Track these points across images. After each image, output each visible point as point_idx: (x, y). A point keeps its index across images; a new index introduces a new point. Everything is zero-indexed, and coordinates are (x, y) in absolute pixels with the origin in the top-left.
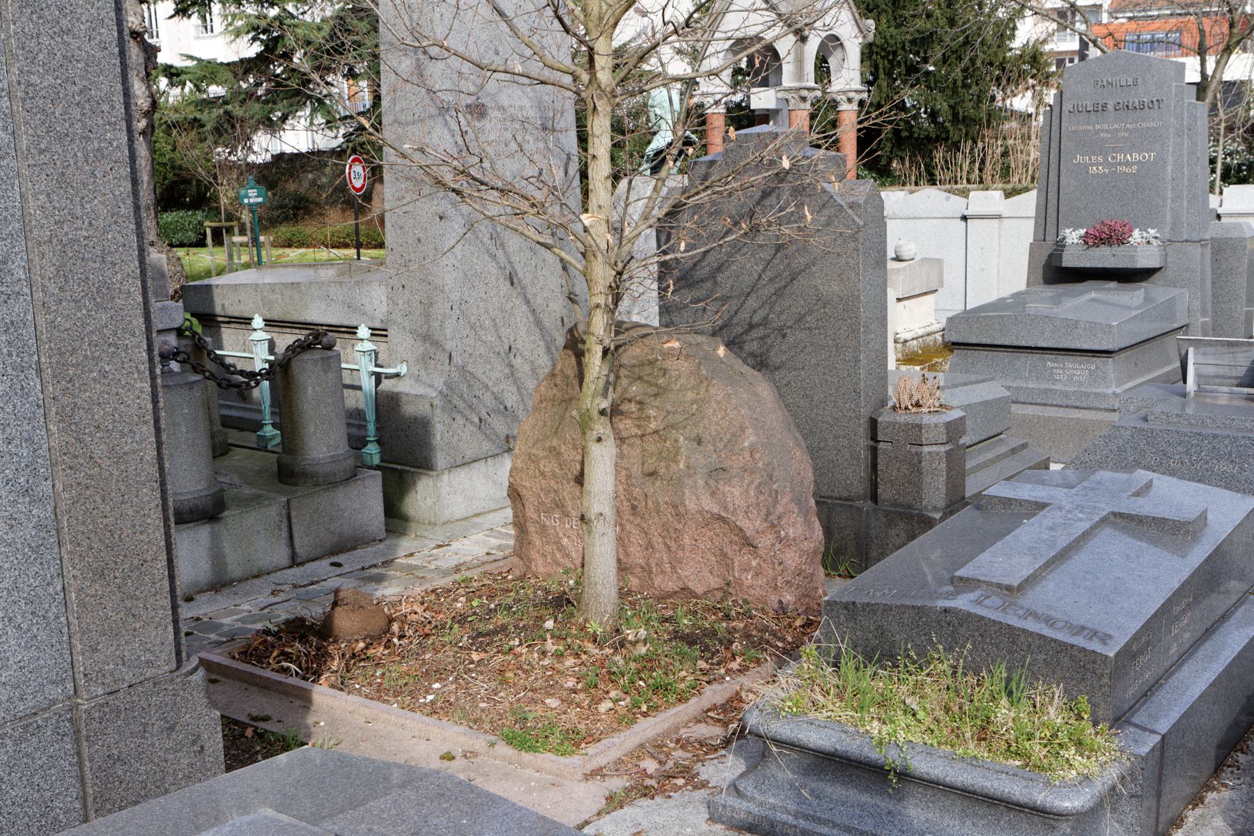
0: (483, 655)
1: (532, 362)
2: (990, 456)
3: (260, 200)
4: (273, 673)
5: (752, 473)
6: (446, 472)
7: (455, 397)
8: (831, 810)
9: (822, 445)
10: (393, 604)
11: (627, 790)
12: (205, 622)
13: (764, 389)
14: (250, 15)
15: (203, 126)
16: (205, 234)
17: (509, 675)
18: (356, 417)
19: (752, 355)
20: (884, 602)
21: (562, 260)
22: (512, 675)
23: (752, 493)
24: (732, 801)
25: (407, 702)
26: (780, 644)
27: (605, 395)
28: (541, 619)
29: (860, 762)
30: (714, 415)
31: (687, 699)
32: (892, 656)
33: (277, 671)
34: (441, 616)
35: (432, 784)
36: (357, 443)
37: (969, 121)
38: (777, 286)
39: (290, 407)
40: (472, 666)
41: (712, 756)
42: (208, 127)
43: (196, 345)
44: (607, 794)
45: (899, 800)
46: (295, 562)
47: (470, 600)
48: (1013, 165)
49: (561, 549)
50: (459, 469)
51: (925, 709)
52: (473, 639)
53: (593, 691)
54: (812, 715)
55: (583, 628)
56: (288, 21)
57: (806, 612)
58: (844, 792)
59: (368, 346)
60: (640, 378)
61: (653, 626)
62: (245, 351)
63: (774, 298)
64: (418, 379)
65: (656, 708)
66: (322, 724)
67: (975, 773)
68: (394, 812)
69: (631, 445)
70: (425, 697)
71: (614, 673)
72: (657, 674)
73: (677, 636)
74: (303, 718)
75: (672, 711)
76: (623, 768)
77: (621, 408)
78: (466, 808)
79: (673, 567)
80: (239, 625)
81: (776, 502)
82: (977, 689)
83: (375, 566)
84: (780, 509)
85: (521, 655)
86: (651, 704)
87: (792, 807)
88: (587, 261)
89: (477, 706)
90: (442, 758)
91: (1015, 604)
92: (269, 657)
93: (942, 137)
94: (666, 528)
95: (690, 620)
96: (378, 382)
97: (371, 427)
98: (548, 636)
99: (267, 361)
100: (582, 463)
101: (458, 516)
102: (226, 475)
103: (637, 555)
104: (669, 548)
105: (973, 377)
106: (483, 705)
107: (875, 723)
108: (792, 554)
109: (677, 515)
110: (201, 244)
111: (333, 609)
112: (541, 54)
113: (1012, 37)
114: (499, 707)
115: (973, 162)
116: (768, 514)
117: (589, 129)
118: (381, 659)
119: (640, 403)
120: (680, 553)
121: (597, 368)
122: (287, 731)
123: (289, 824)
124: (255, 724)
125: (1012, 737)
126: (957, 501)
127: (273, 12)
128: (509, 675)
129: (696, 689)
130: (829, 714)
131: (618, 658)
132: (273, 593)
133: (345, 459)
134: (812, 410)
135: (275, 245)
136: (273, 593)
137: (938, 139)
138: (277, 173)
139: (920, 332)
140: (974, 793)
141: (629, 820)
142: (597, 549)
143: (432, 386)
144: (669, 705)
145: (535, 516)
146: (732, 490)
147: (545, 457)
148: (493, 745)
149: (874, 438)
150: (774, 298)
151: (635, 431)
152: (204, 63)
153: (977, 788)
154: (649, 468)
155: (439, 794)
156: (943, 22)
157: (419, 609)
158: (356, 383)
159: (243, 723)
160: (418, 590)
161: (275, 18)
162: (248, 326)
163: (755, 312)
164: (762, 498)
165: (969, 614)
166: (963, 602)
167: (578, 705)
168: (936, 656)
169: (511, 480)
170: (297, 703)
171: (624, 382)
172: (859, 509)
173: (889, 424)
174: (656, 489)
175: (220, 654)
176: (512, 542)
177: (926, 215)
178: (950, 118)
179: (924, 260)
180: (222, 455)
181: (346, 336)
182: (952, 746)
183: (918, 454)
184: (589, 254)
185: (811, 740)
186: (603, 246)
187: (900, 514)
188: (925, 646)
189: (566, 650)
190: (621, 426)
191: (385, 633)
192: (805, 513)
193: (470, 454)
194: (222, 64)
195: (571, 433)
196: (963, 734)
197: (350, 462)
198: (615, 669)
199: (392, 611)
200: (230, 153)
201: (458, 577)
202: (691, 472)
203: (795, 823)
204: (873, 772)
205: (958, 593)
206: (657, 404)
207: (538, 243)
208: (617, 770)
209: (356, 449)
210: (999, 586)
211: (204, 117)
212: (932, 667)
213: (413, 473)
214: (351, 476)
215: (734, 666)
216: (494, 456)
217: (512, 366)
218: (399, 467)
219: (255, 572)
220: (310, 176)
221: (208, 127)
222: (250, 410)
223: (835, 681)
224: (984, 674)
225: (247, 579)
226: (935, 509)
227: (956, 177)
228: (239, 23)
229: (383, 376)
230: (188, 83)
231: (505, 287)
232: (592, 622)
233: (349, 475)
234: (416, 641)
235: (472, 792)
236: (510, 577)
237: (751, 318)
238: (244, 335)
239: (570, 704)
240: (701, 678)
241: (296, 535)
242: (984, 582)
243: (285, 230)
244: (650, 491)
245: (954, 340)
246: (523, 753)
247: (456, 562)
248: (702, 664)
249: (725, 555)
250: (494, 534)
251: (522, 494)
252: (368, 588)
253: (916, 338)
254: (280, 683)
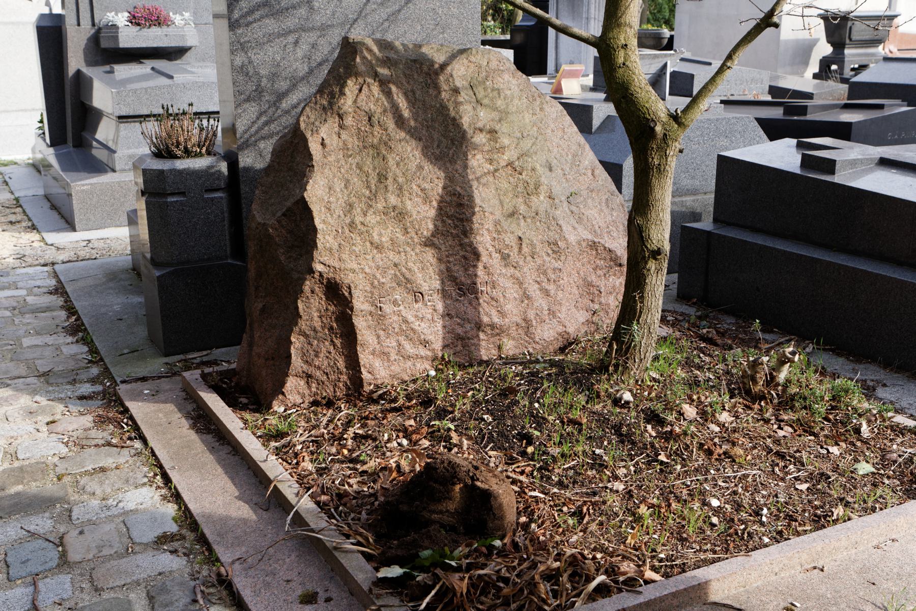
63: (386, 24)
94: (542, 270)
150: (386, 24)
154: (508, 207)
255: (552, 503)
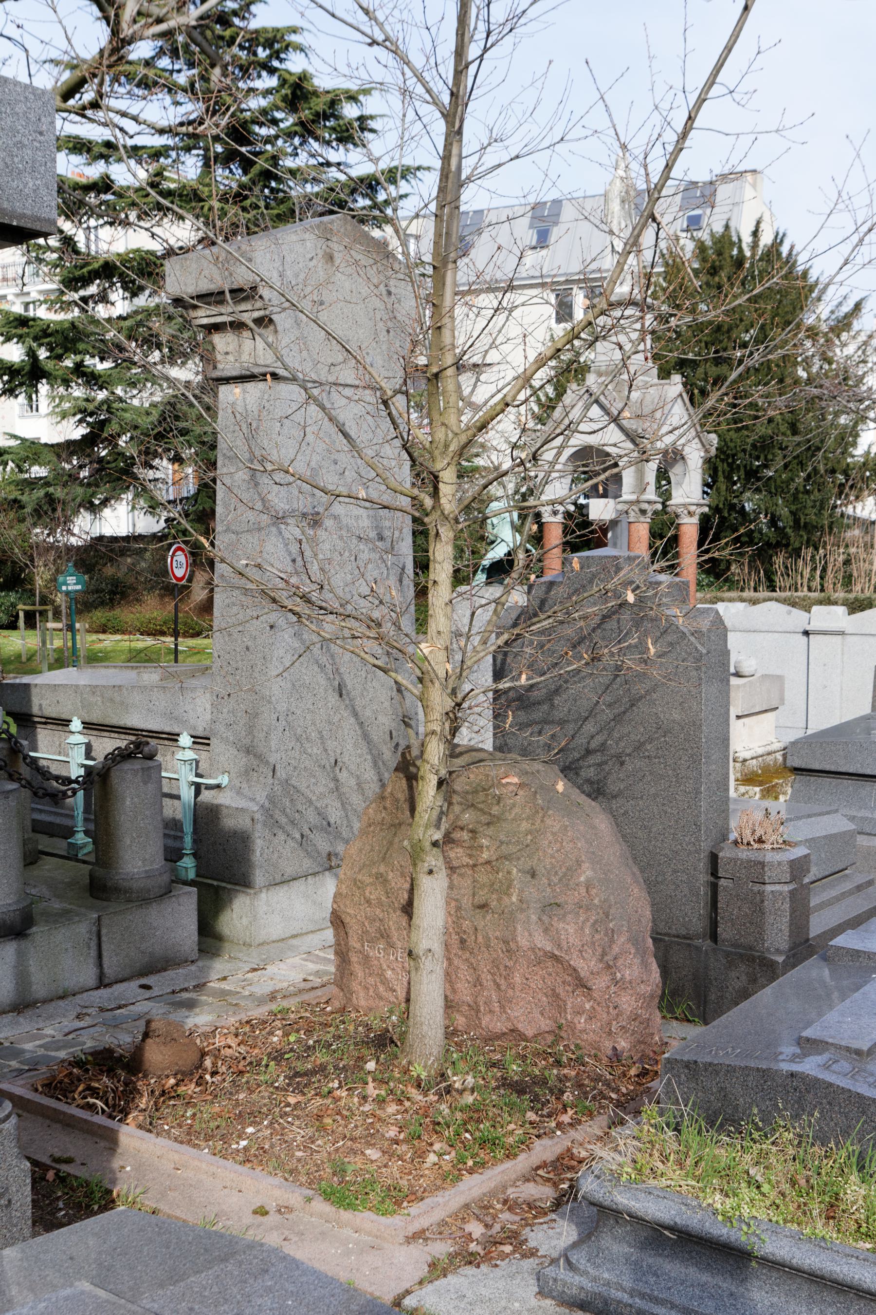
0: (300, 1098)
1: (358, 777)
2: (834, 893)
3: (79, 587)
4: (78, 1110)
5: (588, 909)
6: (264, 890)
7: (277, 812)
8: (669, 1289)
9: (660, 879)
10: (206, 1036)
11: (452, 1257)
12: (7, 1047)
13: (603, 823)
14: (78, 398)
15: (22, 507)
16: (17, 617)
17: (328, 1121)
18: (173, 827)
19: (589, 781)
20: (727, 1063)
21: (396, 682)
22: (330, 1121)
23: (587, 931)
24: (562, 1272)
25: (219, 1148)
26: (614, 1096)
27: (438, 827)
28: (361, 1059)
29: (701, 1238)
30: (549, 847)
31: (516, 1155)
32: (734, 1121)
33: (82, 1108)
34: (256, 1051)
35: (255, 1257)
36: (173, 855)
37: (810, 528)
38: (616, 711)
39: (107, 818)
40: (288, 1109)
41: (541, 1220)
42: (28, 510)
43: (12, 748)
44: (430, 1260)
45: (742, 1281)
46: (102, 983)
47: (287, 1034)
48: (855, 574)
49: (385, 981)
50: (277, 887)
51: (769, 1182)
52: (290, 1078)
53: (415, 1142)
54: (652, 1182)
55: (406, 1071)
56: (115, 405)
57: (641, 1060)
58: (683, 1270)
59: (190, 755)
60: (473, 805)
61: (481, 1072)
62: (60, 754)
63: (613, 723)
64: (239, 792)
65: (483, 1165)
66: (128, 1169)
67: (823, 1256)
68: (215, 1289)
69: (462, 875)
70: (238, 1143)
71: (439, 1124)
72: (485, 1126)
73: (505, 1083)
74: (109, 1161)
75: (500, 1168)
76: (447, 1231)
77: (452, 836)
78: (291, 1288)
79: (502, 1007)
80: (42, 1052)
81: (612, 941)
82: (825, 1161)
83: (186, 990)
84: (616, 949)
85: (340, 1099)
86: (478, 1160)
87: (628, 1284)
88: (424, 686)
89: (293, 1156)
90: (255, 1212)
91: (865, 1071)
92: (74, 1091)
93: (781, 543)
94: (496, 963)
95: (520, 1066)
96: (198, 793)
97: (188, 840)
98: (370, 1079)
99: (83, 766)
100: (411, 891)
101: (275, 937)
102: (35, 886)
103: (465, 993)
104: (498, 986)
105: (817, 808)
106: (299, 1154)
107: (718, 1197)
108: (628, 998)
109: (508, 951)
110: (12, 626)
111: (143, 1040)
112: (384, 476)
113: (854, 444)
114: (316, 1156)
115: (814, 569)
116: (604, 954)
117: (430, 554)
118: (191, 1097)
119: (472, 831)
120: (510, 992)
121: (431, 798)
122: (91, 1176)
123: (107, 1301)
124: (58, 1166)
125: (862, 1216)
126: (801, 944)
127: (102, 395)
128: (328, 1121)
129: (525, 1144)
130: (669, 1182)
131: (444, 1108)
132: (78, 1017)
133: (160, 874)
134: (650, 841)
135: (91, 631)
136: (78, 1017)
137: (778, 545)
138: (95, 556)
139: (760, 751)
140: (822, 1278)
141: (452, 1290)
142: (424, 988)
143: (254, 800)
144: (496, 1161)
145: (358, 946)
146: (567, 927)
147: (371, 884)
148: (309, 1200)
149: (714, 873)
150: (613, 723)
151: (466, 860)
152: (28, 444)
153: (825, 1272)
154: (479, 900)
155: (263, 1270)
156: (783, 428)
157: (232, 1041)
158: (175, 792)
159: (44, 1164)
160: (232, 1020)
161: (103, 402)
162: (66, 728)
163: (592, 737)
164: (597, 937)
165: (817, 1080)
166: (810, 1066)
167: (400, 1158)
168: (782, 1123)
169: (335, 906)
170: (103, 1144)
171: (457, 809)
172: (698, 949)
173: (731, 859)
174: (486, 923)
175: (21, 1086)
176: (332, 969)
177: (766, 628)
178: (791, 524)
179: (765, 676)
180: (31, 863)
181: (166, 742)
182: (799, 1224)
183: (761, 893)
184: (426, 678)
185: (650, 1211)
186: (442, 674)
187: (741, 956)
188: (770, 1112)
189: (388, 1095)
190: (452, 855)
191: (197, 1068)
192: (641, 952)
193: (289, 871)
194: (46, 445)
195: (400, 860)
196: (810, 1211)
197: (166, 878)
198: (440, 1119)
199: (205, 1044)
200: (48, 535)
201: (274, 1007)
202: (524, 906)
203: (630, 1301)
204: (715, 1249)
205: (805, 1055)
206: (491, 833)
207: (374, 666)
208: (440, 1233)
209: (171, 861)
210: (848, 1049)
211: (25, 498)
212: (777, 1135)
213: (229, 890)
214: (166, 893)
215: (566, 1118)
216: (314, 874)
217: (337, 781)
218: (215, 883)
219: (60, 993)
220: (129, 560)
221: (28, 510)
222: (61, 815)
223: (675, 1146)
224: (832, 1145)
225: (52, 1000)
226: (778, 951)
227: (797, 584)
228: (66, 405)
229: (203, 787)
230: (11, 464)
231: (333, 698)
232: (416, 1065)
233: (163, 891)
234: (229, 1079)
235: (298, 1268)
236: (329, 1009)
237: (588, 743)
238: (60, 737)
239: (391, 1156)
240: (531, 1131)
241: (105, 954)
242: (832, 1044)
243: (100, 615)
244: (481, 925)
245: (796, 765)
246: (341, 1211)
247: (271, 989)
248: (531, 1116)
249: (558, 996)
250: (311, 958)
251: (346, 921)
252: (177, 1016)
253: (756, 758)
254: (85, 1121)
255: (745, 1228)
